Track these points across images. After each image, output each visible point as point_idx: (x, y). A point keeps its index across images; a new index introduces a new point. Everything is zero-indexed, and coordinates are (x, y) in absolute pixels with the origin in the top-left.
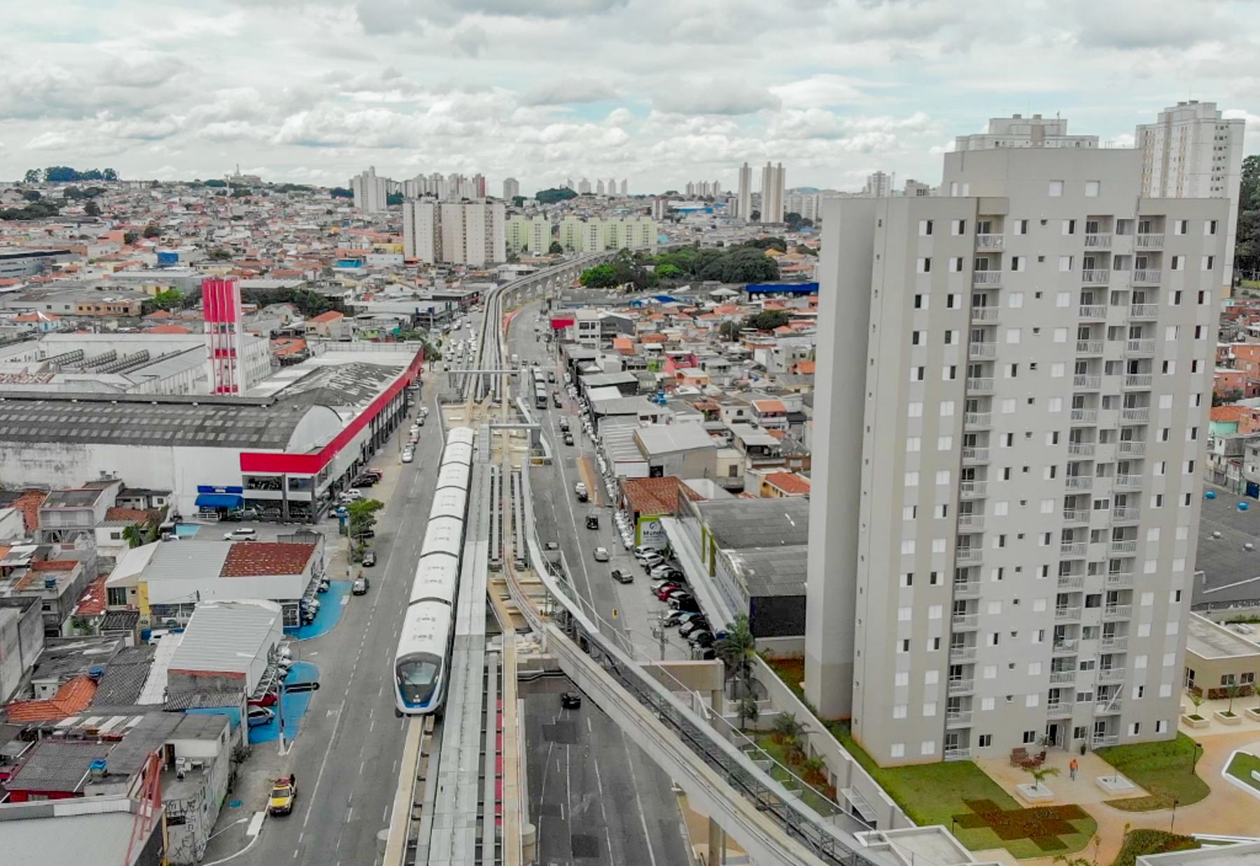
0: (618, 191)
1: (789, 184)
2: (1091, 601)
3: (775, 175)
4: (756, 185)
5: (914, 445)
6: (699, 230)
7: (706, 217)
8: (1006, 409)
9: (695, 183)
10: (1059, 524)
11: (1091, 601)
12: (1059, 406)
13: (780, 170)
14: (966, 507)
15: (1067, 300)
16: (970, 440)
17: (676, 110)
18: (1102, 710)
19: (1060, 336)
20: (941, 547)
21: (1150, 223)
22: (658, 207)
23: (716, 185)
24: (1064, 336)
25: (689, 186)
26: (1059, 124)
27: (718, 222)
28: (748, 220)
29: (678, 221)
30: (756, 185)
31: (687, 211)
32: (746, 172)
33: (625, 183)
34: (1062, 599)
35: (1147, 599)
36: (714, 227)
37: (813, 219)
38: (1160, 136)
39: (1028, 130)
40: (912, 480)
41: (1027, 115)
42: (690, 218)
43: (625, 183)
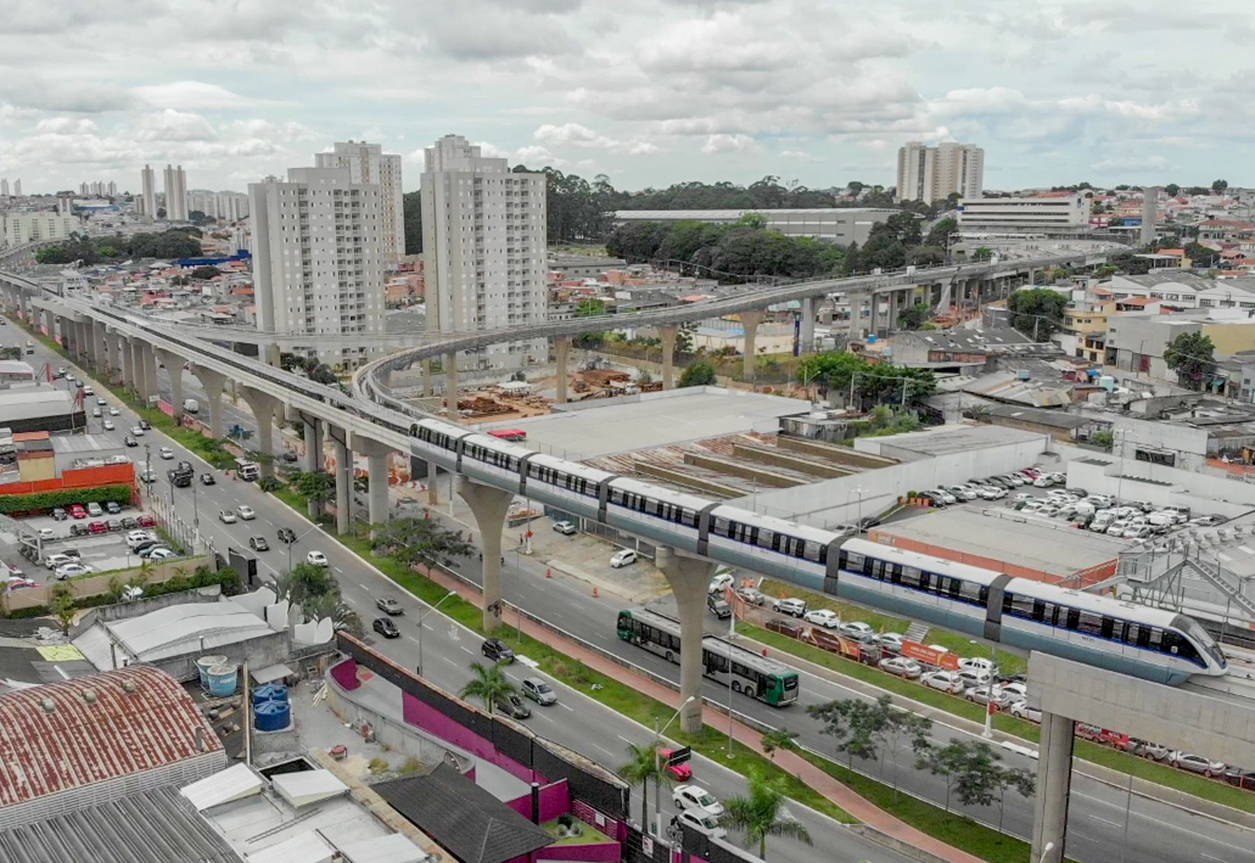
0: (12, 193)
1: (190, 185)
2: (352, 318)
3: (175, 176)
4: (160, 187)
5: (287, 264)
6: (109, 226)
7: (114, 215)
8: (315, 253)
9: (89, 183)
10: (338, 293)
11: (352, 318)
12: (333, 252)
13: (180, 173)
14: (307, 286)
15: (331, 217)
16: (305, 263)
17: (33, 105)
18: (360, 356)
19: (330, 229)
20: (300, 299)
21: (354, 192)
22: (64, 204)
23: (111, 185)
24: (332, 229)
25: (83, 187)
26: (377, 148)
27: (126, 219)
28: (155, 217)
29: (87, 218)
30: (160, 187)
31: (94, 209)
32: (148, 174)
33: (18, 183)
34: (343, 318)
35: (370, 318)
36: (123, 223)
37: (216, 216)
38: (437, 156)
39: (358, 151)
40: (288, 276)
41: (357, 141)
42: (98, 215)
43: (18, 183)
